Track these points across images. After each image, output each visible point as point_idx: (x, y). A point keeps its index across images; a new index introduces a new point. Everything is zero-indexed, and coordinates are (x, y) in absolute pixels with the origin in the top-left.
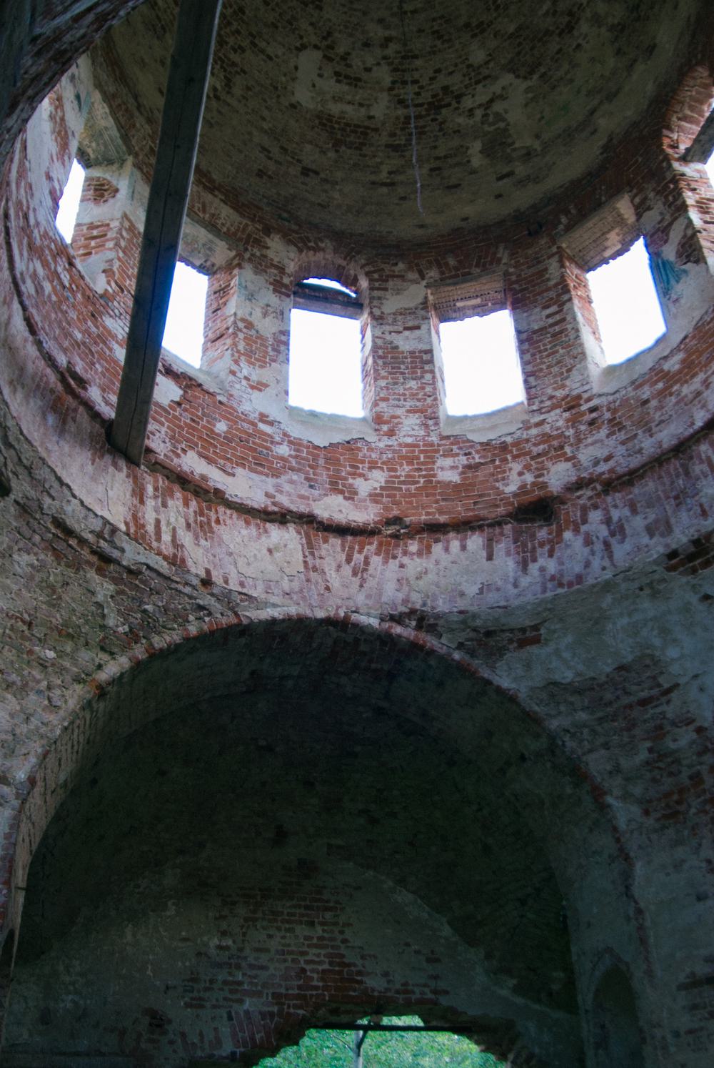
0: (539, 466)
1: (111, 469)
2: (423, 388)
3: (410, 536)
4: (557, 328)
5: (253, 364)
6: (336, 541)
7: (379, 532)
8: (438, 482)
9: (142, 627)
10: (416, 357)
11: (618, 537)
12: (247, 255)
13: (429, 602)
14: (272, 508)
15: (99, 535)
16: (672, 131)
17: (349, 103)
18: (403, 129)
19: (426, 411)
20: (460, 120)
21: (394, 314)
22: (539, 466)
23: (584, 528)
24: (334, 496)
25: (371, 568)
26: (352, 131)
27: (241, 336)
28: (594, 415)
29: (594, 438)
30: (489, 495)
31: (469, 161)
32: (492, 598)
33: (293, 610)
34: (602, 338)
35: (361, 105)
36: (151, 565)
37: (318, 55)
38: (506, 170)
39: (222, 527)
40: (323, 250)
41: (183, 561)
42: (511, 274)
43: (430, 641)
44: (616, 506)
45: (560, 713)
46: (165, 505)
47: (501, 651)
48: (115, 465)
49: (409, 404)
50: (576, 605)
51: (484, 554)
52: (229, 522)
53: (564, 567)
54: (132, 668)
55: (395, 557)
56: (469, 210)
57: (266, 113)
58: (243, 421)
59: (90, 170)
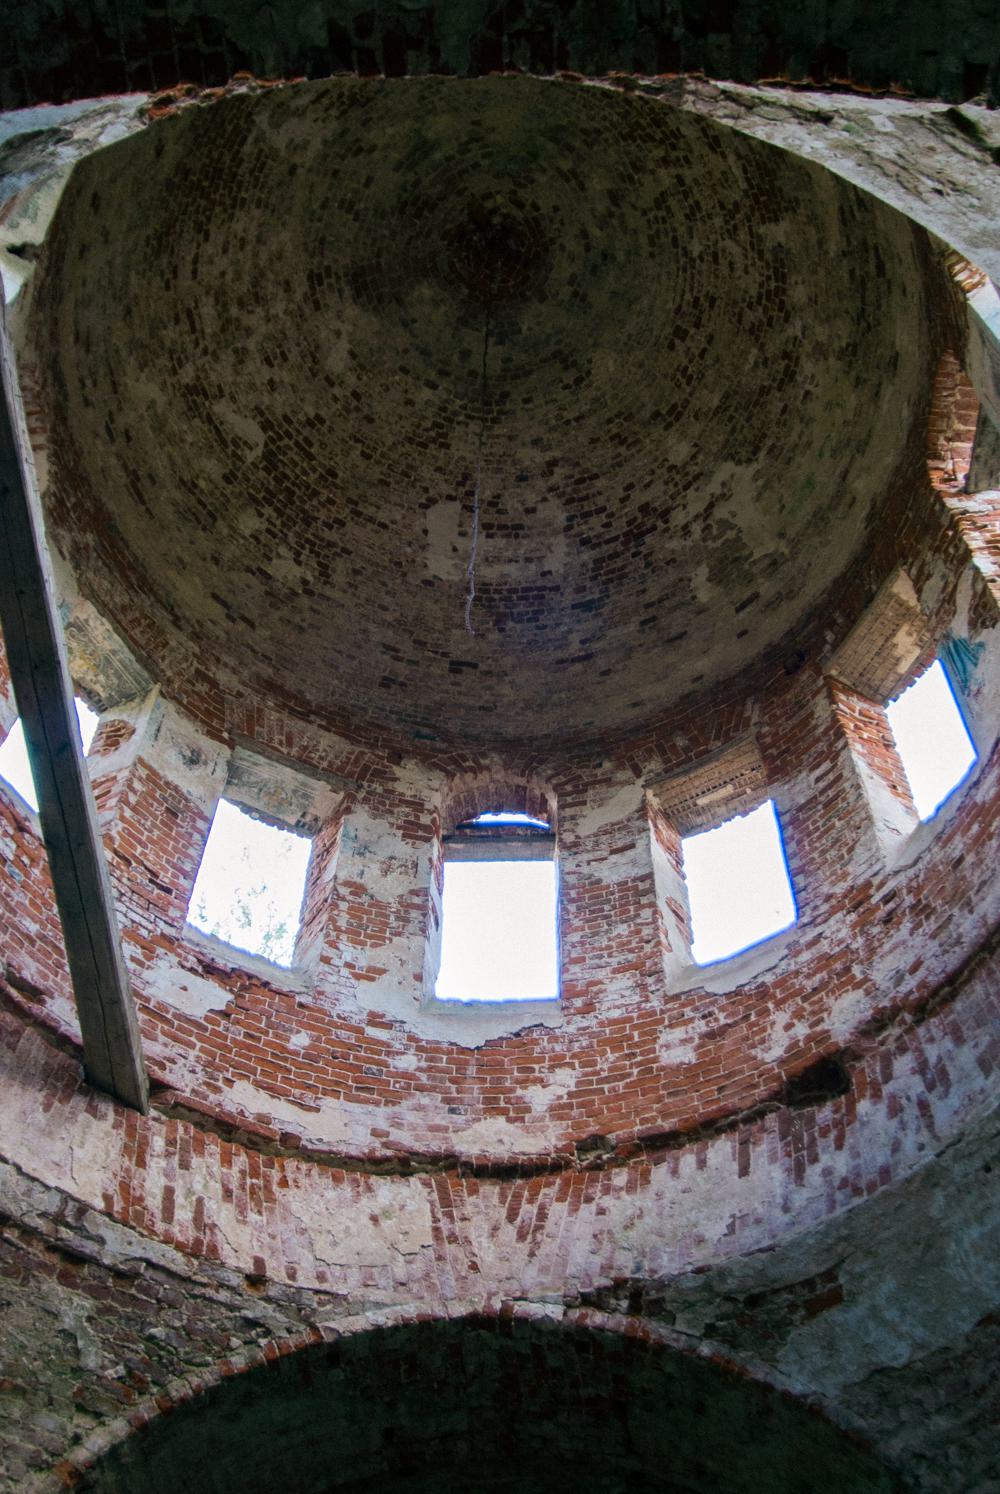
0: (816, 1007)
1: (83, 1117)
2: (638, 932)
3: (617, 1162)
4: (831, 793)
5: (363, 944)
6: (490, 1190)
7: (568, 1165)
8: (662, 1068)
9: (148, 1366)
10: (628, 890)
11: (940, 1089)
12: (361, 795)
13: (646, 1265)
14: (381, 1152)
15: (58, 1219)
16: (943, 460)
17: (510, 561)
18: (593, 579)
19: (644, 964)
20: (674, 544)
21: (595, 835)
22: (816, 1007)
23: (887, 1089)
24: (490, 1120)
25: (549, 1225)
26: (520, 598)
27: (344, 906)
28: (891, 905)
29: (894, 940)
30: (741, 1071)
31: (694, 598)
32: (750, 1237)
33: (411, 1310)
34: (914, 792)
35: (529, 560)
36: (154, 1260)
37: (456, 506)
38: (747, 594)
39: (291, 1192)
40: (488, 768)
41: (213, 1249)
42: (765, 736)
43: (656, 1330)
44: (932, 1040)
45: (903, 1423)
46: (185, 1165)
47: (781, 1327)
48: (93, 1110)
49: (614, 962)
50: (888, 1224)
51: (735, 1166)
52: (303, 1181)
53: (861, 1161)
54: (131, 1437)
55: (589, 1200)
56: (703, 665)
57: (387, 600)
58: (340, 1027)
59: (104, 715)
